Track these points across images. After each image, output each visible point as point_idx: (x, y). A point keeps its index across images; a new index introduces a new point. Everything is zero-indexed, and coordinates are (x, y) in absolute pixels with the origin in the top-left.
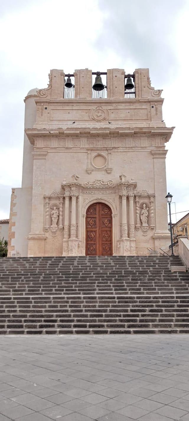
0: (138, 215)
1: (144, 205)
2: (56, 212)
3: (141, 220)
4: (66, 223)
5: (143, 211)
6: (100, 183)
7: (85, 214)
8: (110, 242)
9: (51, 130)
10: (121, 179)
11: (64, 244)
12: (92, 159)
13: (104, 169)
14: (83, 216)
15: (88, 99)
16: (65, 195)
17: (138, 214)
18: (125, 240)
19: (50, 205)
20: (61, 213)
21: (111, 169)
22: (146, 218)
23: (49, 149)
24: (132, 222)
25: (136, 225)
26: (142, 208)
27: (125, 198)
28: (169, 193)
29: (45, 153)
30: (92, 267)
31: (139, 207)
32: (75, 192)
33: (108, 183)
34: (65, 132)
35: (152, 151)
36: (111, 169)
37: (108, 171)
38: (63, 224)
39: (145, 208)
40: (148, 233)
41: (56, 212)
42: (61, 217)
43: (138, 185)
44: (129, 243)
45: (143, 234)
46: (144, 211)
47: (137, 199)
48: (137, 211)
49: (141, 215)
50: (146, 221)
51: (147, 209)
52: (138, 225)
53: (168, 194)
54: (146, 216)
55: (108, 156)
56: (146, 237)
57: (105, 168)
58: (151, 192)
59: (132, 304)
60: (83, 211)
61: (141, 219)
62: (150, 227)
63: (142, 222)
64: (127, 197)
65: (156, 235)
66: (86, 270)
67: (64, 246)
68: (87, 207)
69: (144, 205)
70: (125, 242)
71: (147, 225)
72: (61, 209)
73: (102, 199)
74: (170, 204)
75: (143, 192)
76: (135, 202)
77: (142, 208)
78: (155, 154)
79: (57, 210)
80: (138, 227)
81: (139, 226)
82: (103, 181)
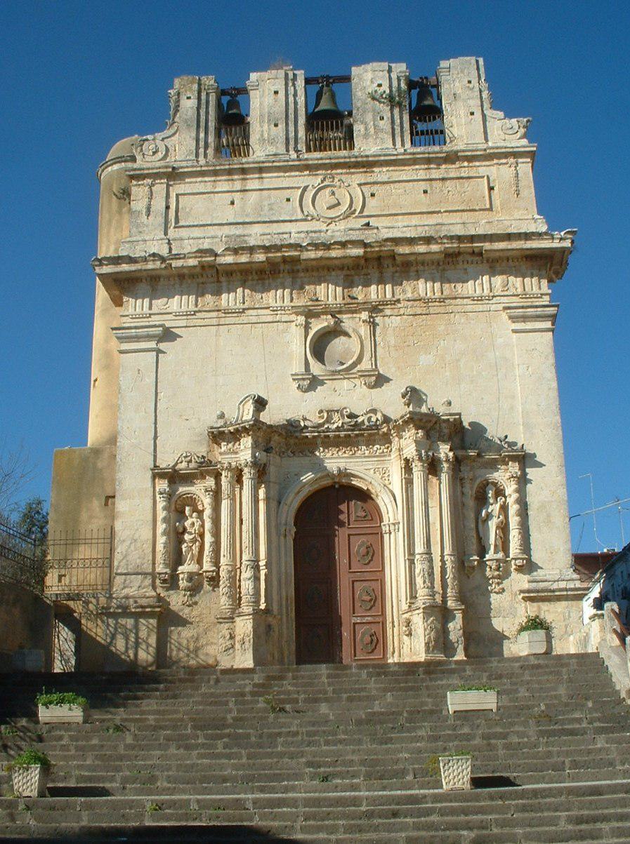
38: (216, 563)
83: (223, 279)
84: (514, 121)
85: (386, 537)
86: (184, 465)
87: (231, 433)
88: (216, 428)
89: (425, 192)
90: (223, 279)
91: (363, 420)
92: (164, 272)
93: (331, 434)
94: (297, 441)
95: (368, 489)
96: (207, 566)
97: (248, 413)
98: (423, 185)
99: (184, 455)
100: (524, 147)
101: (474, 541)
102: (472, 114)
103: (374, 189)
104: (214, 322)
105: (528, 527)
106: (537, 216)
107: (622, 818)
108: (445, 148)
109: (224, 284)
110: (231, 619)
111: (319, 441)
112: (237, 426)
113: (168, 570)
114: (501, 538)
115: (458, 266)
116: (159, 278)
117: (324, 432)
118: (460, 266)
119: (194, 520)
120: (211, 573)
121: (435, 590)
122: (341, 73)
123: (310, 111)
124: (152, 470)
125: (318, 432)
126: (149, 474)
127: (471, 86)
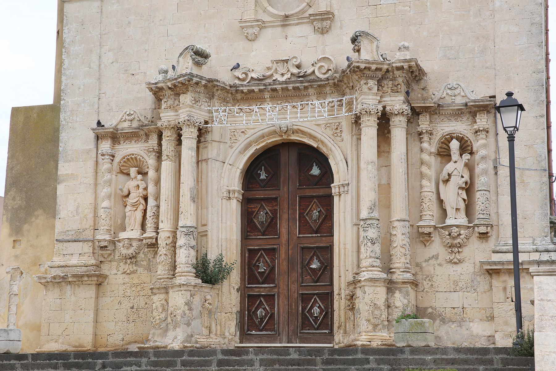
0: (429, 186)
1: (455, 145)
2: (138, 186)
4: (165, 226)
5: (449, 167)
16: (159, 124)
17: (430, 180)
19: (117, 159)
20: (151, 189)
22: (464, 193)
28: (510, 94)
31: (430, 154)
39: (455, 155)
40: (466, 252)
41: (138, 186)
43: (212, 61)
46: (455, 166)
49: (441, 184)
50: (462, 205)
53: (505, 97)
56: (458, 268)
61: (442, 198)
62: (473, 227)
63: (445, 211)
69: (455, 145)
70: (366, 289)
72: (151, 174)
73: (303, 133)
74: (511, 139)
75: (449, 91)
81: (430, 227)
85: (336, 199)
86: (126, 125)
87: (170, 88)
88: (153, 84)
91: (314, 71)
94: (243, 95)
95: (318, 147)
96: (150, 233)
99: (128, 113)
105: (57, 130)
107: (553, 262)
110: (166, 290)
112: (175, 81)
114: (464, 200)
117: (270, 85)
119: (139, 183)
120: (150, 240)
122: (510, 142)
124: (93, 129)
125: (265, 85)
126: (92, 135)
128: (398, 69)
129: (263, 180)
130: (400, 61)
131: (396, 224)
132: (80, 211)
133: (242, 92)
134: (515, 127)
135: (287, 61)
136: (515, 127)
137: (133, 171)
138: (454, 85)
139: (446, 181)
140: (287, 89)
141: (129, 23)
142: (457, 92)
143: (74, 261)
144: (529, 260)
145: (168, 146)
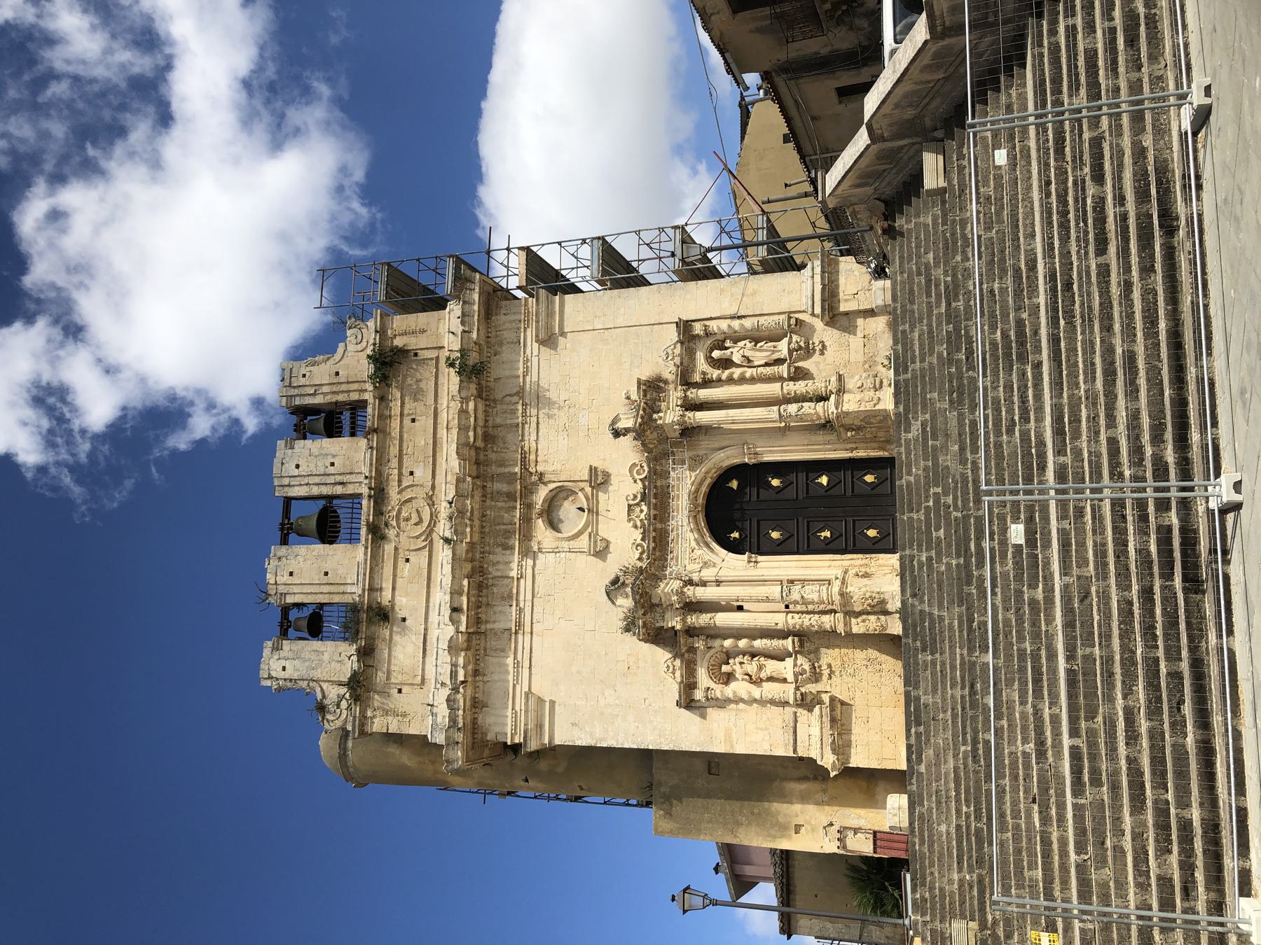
0: (749, 373)
1: (716, 354)
3: (767, 365)
5: (736, 358)
6: (638, 504)
7: (745, 557)
8: (851, 547)
9: (456, 680)
10: (626, 431)
11: (855, 630)
12: (560, 535)
13: (590, 495)
14: (752, 564)
15: (362, 555)
18: (837, 408)
21: (593, 471)
22: (759, 345)
23: (518, 687)
24: (774, 389)
25: (791, 702)
26: (726, 363)
27: (689, 414)
29: (532, 702)
30: (939, 490)
32: (668, 588)
33: (637, 477)
34: (463, 628)
35: (537, 336)
36: (593, 471)
37: (599, 480)
38: (783, 634)
42: (759, 644)
44: (846, 397)
45: (817, 352)
47: (697, 378)
48: (736, 376)
51: (728, 344)
52: (783, 370)
54: (755, 345)
55: (550, 482)
57: (588, 490)
58: (672, 334)
59: (1089, 533)
60: (734, 564)
64: (687, 410)
65: (818, 310)
66: (938, 219)
67: (862, 631)
68: (723, 552)
69: (716, 354)
71: (786, 340)
76: (707, 383)
77: (726, 363)
78: (549, 327)
79: (731, 661)
80: (792, 369)
82: (632, 497)
83: (483, 628)
84: (349, 333)
86: (678, 674)
89: (413, 421)
90: (483, 628)
92: (469, 692)
93: (653, 512)
96: (788, 643)
97: (627, 441)
98: (407, 421)
100: (376, 323)
101: (768, 369)
102: (326, 574)
103: (405, 472)
104: (527, 638)
106: (448, 309)
108: (371, 400)
109: (489, 626)
111: (659, 526)
113: (790, 639)
115: (492, 387)
116: (475, 698)
118: (491, 384)
121: (816, 600)
123: (307, 635)
127: (308, 374)
128: (645, 395)
129: (740, 535)
130: (638, 392)
131: (785, 391)
132: (764, 727)
133: (654, 549)
134: (704, 897)
135: (629, 506)
136: (704, 897)
137: (725, 668)
138: (663, 354)
139: (749, 361)
140: (655, 505)
141: (578, 672)
142: (670, 352)
143: (815, 731)
144: (791, 754)
145: (703, 619)
